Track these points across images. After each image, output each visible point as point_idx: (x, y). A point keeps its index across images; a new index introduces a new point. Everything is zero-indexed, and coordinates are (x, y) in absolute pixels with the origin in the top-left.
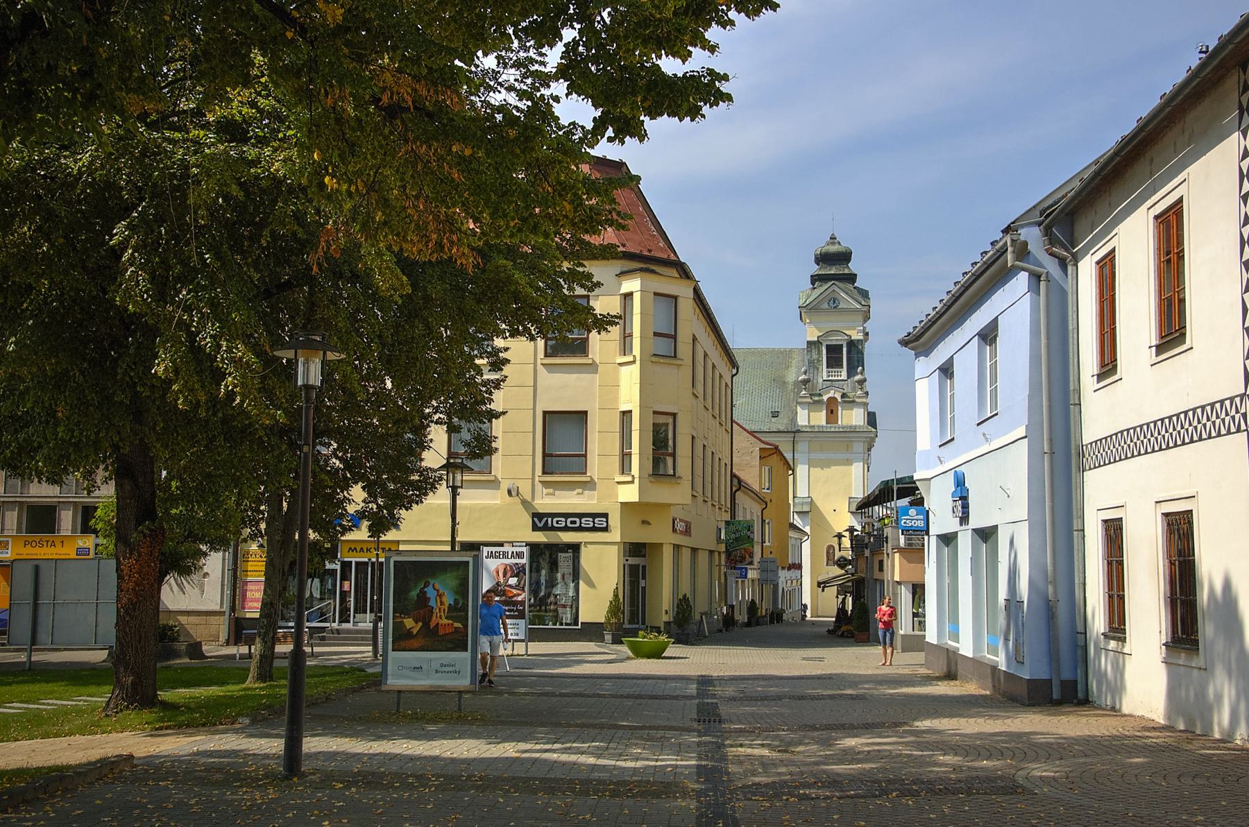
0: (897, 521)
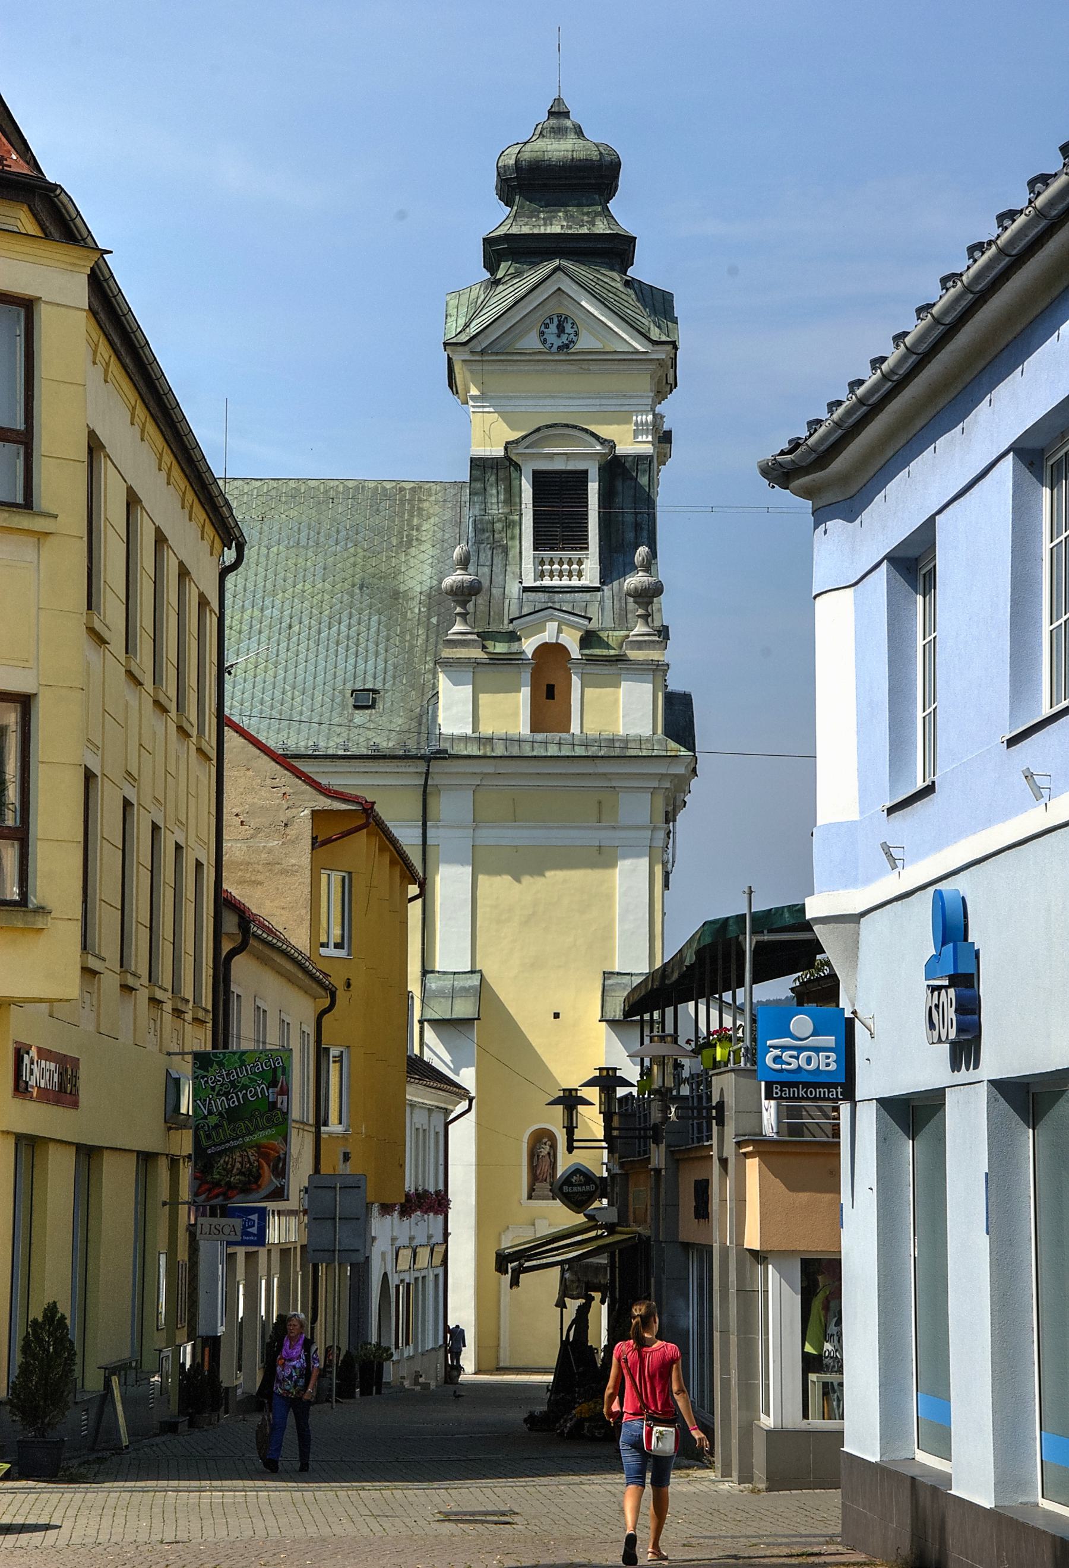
0: (753, 1055)
